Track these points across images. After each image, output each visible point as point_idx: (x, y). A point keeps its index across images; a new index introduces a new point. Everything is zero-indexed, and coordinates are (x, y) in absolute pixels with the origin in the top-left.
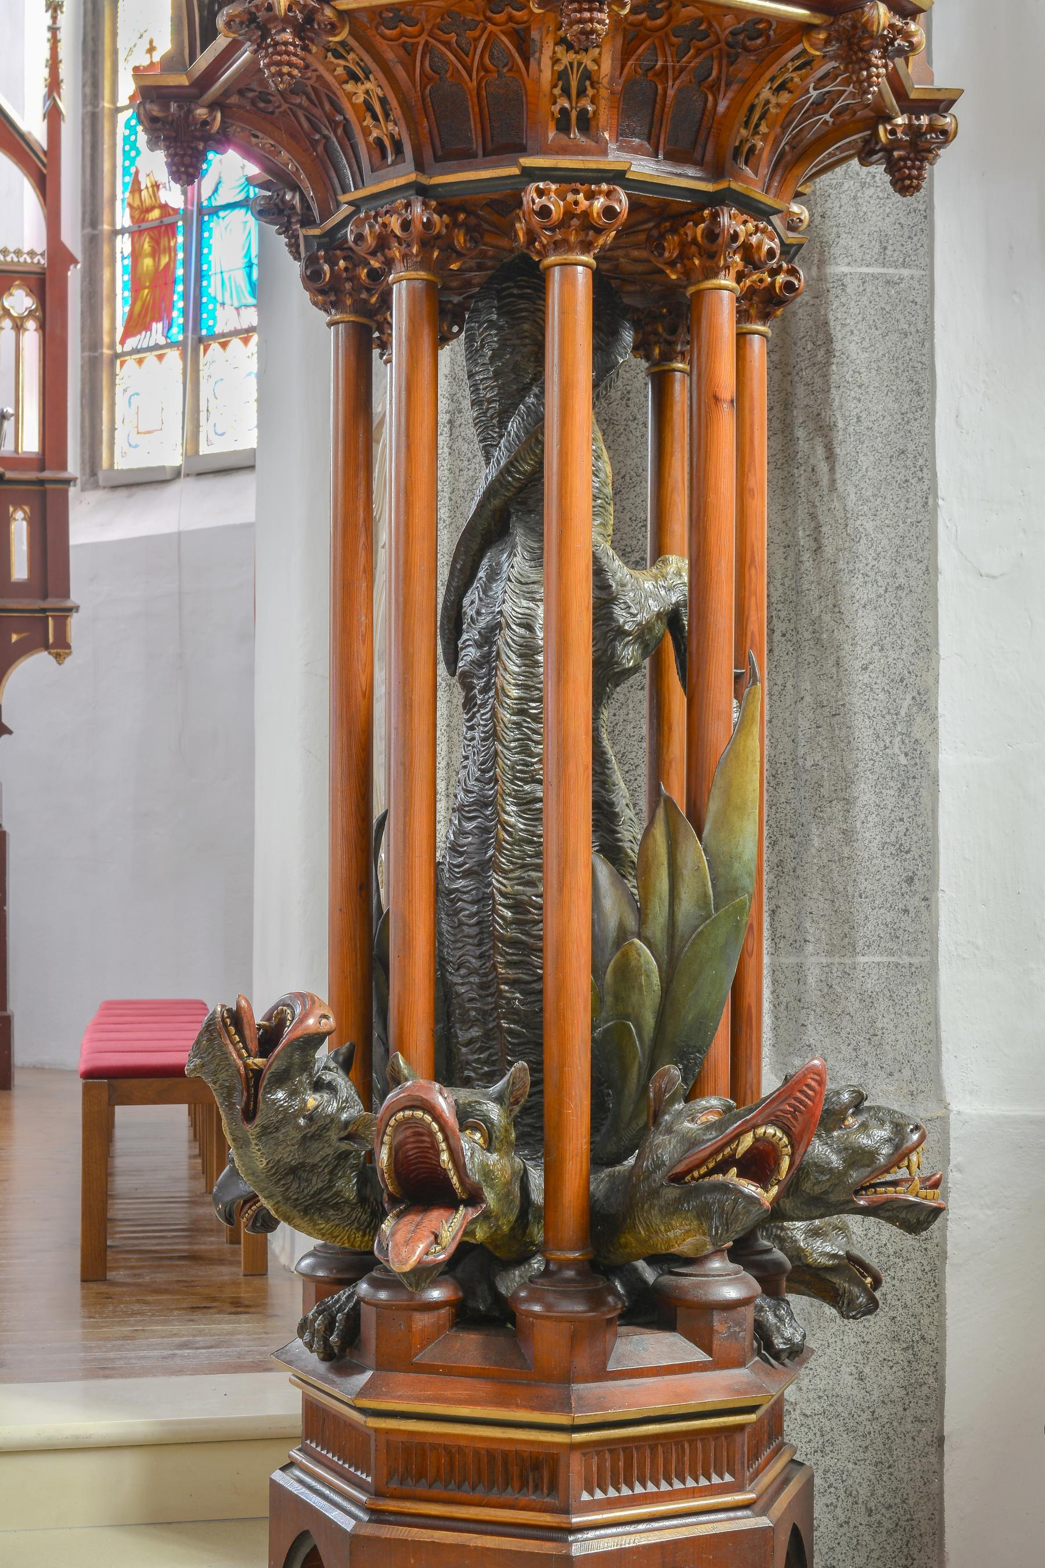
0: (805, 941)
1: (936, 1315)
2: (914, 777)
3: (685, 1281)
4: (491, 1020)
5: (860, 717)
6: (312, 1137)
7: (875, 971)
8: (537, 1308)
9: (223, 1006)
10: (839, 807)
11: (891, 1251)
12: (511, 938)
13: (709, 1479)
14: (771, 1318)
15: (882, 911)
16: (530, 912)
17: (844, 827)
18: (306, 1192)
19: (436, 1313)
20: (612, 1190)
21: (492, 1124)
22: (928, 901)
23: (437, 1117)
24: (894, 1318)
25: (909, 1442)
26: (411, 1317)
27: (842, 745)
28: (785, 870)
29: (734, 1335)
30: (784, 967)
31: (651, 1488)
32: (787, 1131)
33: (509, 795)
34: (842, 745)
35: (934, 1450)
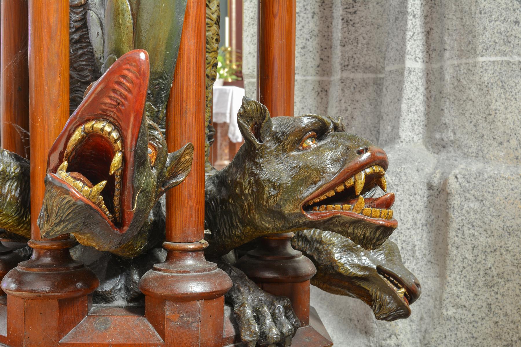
0: (445, 49)
7: (491, 67)
11: (495, 273)
15: (498, 23)
28: (436, 3)
30: (434, 70)
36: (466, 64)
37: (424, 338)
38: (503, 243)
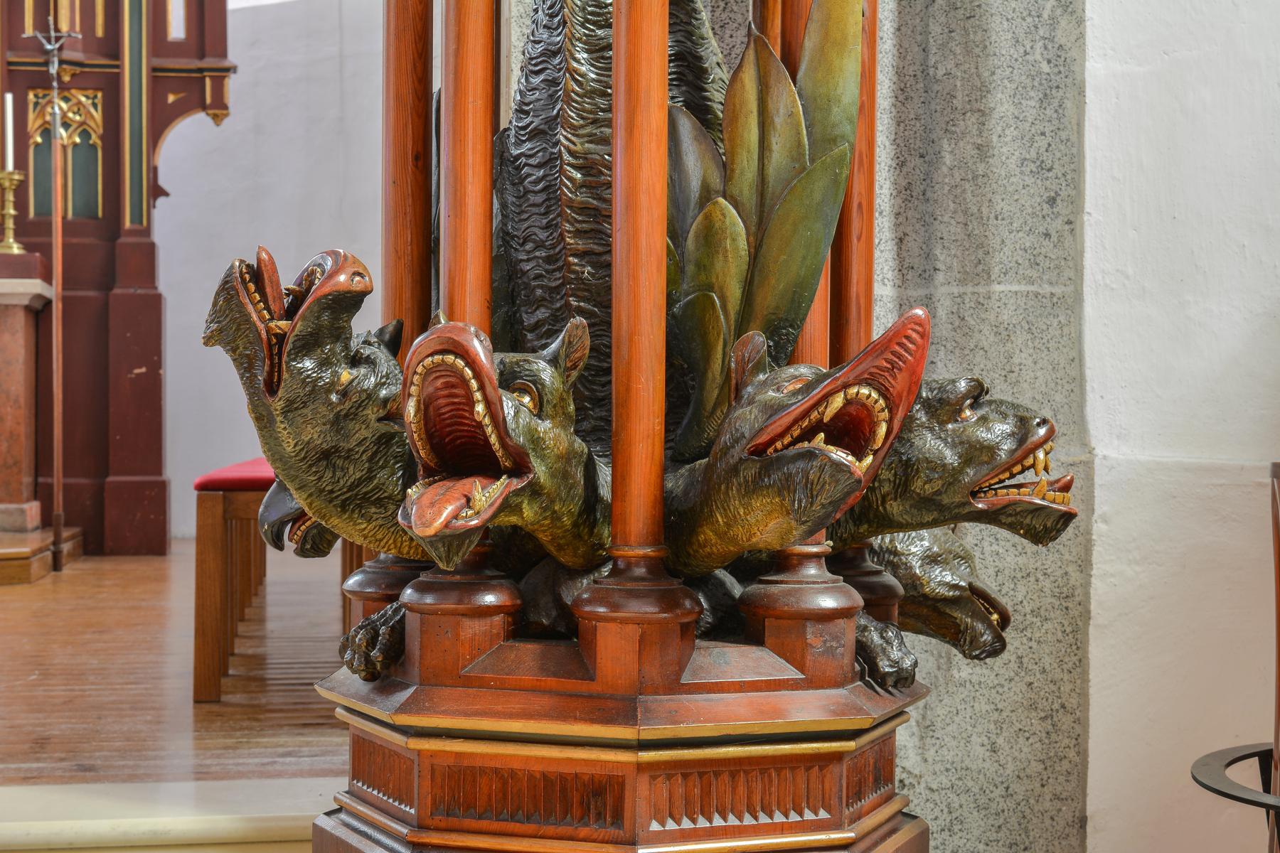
0: (935, 269)
1: (1079, 682)
2: (1058, 87)
3: (774, 589)
4: (547, 278)
5: (997, 19)
6: (346, 416)
7: (1012, 301)
8: (602, 610)
9: (242, 261)
10: (973, 120)
11: (1028, 610)
12: (582, 202)
13: (801, 814)
14: (876, 638)
15: (1021, 234)
16: (601, 173)
17: (979, 141)
18: (342, 482)
19: (488, 621)
20: (690, 485)
21: (543, 385)
22: (1073, 224)
23: (471, 362)
24: (1031, 684)
25: (1048, 822)
26: (458, 623)
27: (977, 50)
29: (830, 651)
31: (732, 820)
32: (884, 393)
33: (579, 40)
34: (977, 50)
35: (1075, 831)
36: (974, 293)
37: (924, 717)
38: (1039, 564)
